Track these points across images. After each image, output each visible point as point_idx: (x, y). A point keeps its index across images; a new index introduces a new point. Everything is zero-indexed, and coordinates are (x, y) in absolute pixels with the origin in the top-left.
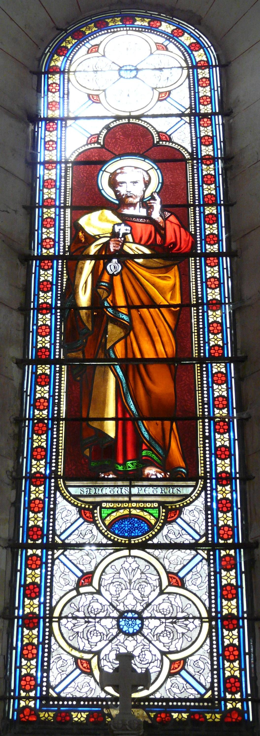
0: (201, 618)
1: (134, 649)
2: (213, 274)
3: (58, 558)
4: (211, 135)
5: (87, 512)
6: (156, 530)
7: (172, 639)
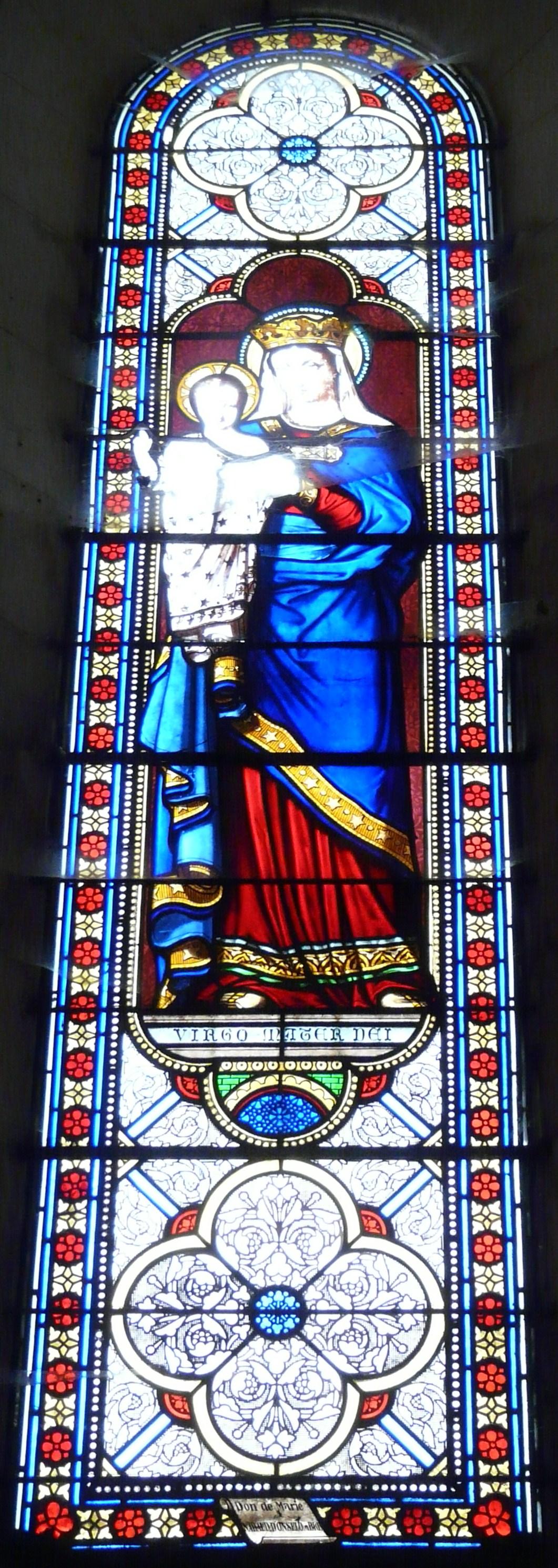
2: (482, 976)
3: (126, 1176)
4: (472, 287)
5: (189, 1085)
7: (367, 1347)
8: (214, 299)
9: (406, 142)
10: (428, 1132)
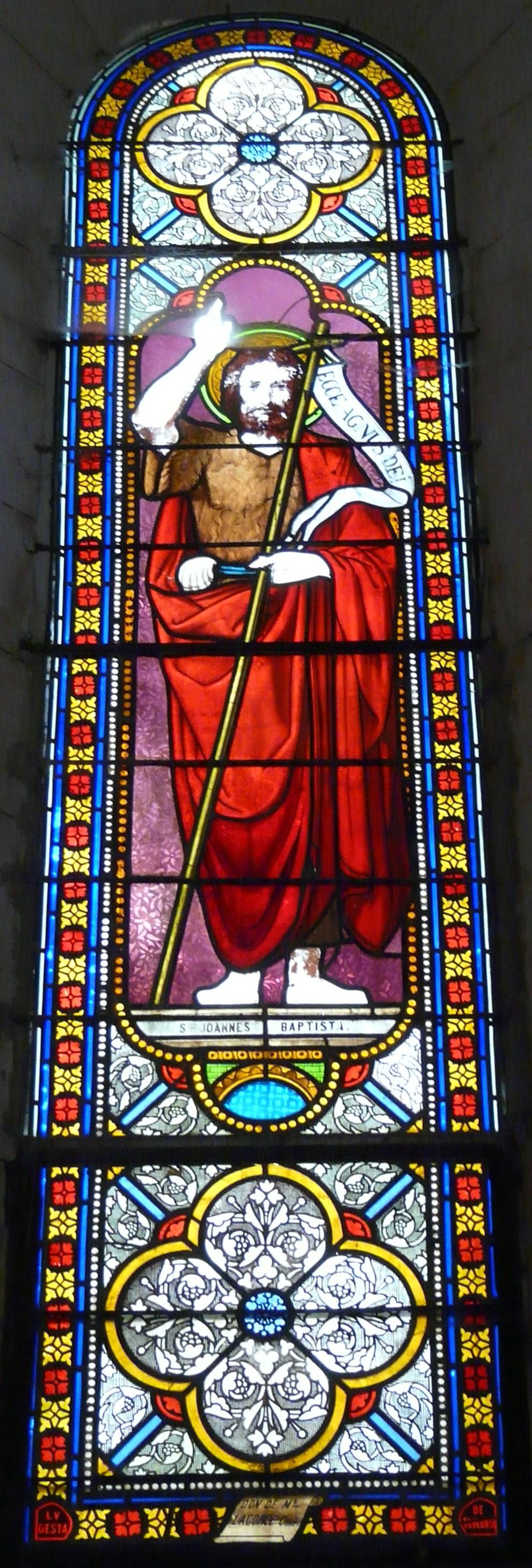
0: (370, 142)
1: (275, 1370)
9: (365, 139)
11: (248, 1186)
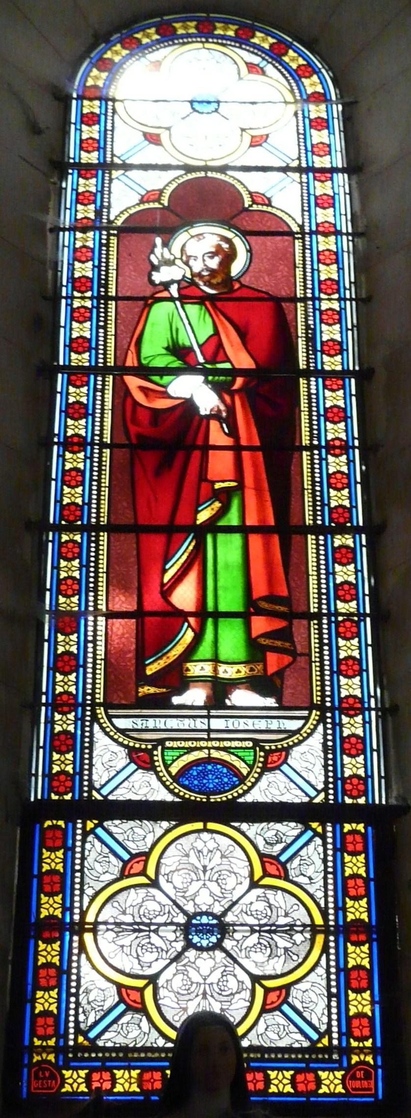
6: (249, 784)
8: (147, 206)
10: (316, 793)
11: (192, 837)
